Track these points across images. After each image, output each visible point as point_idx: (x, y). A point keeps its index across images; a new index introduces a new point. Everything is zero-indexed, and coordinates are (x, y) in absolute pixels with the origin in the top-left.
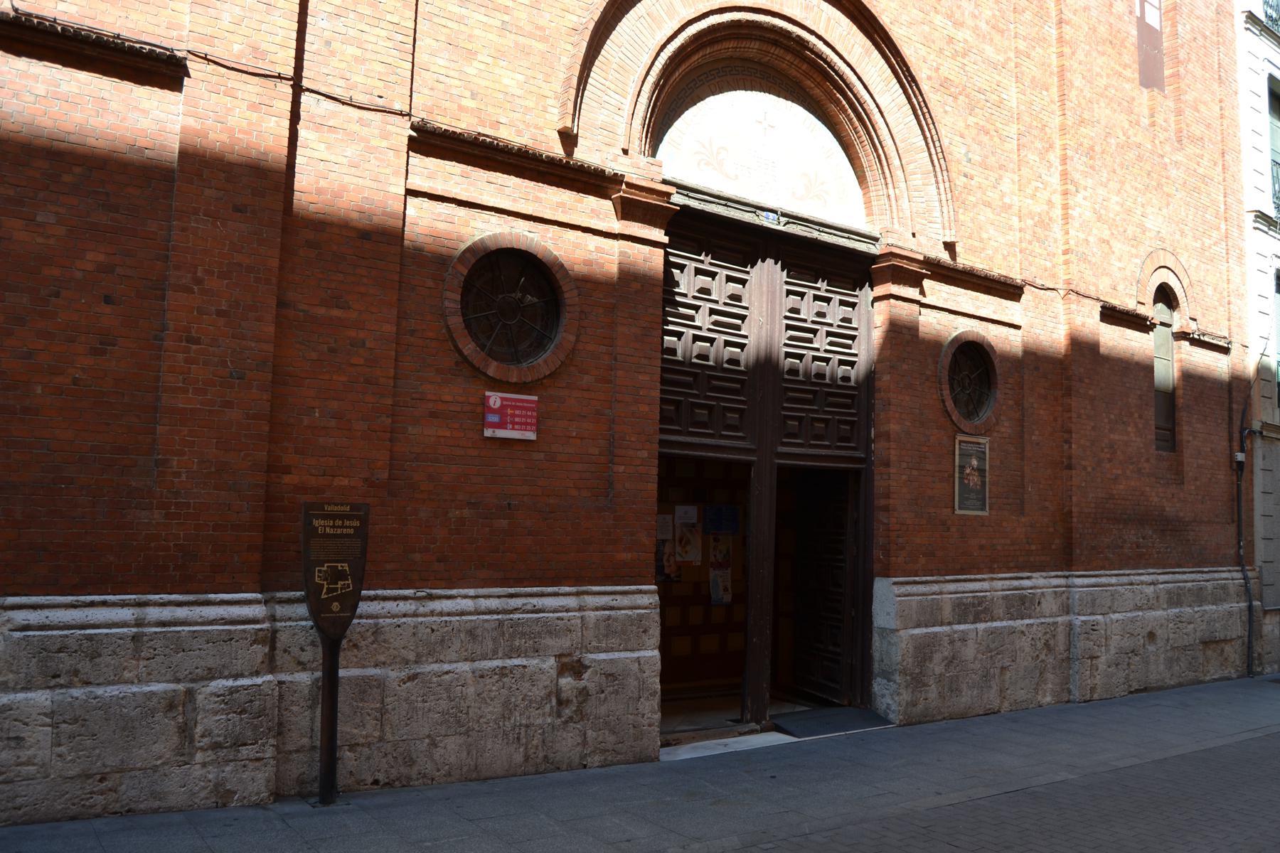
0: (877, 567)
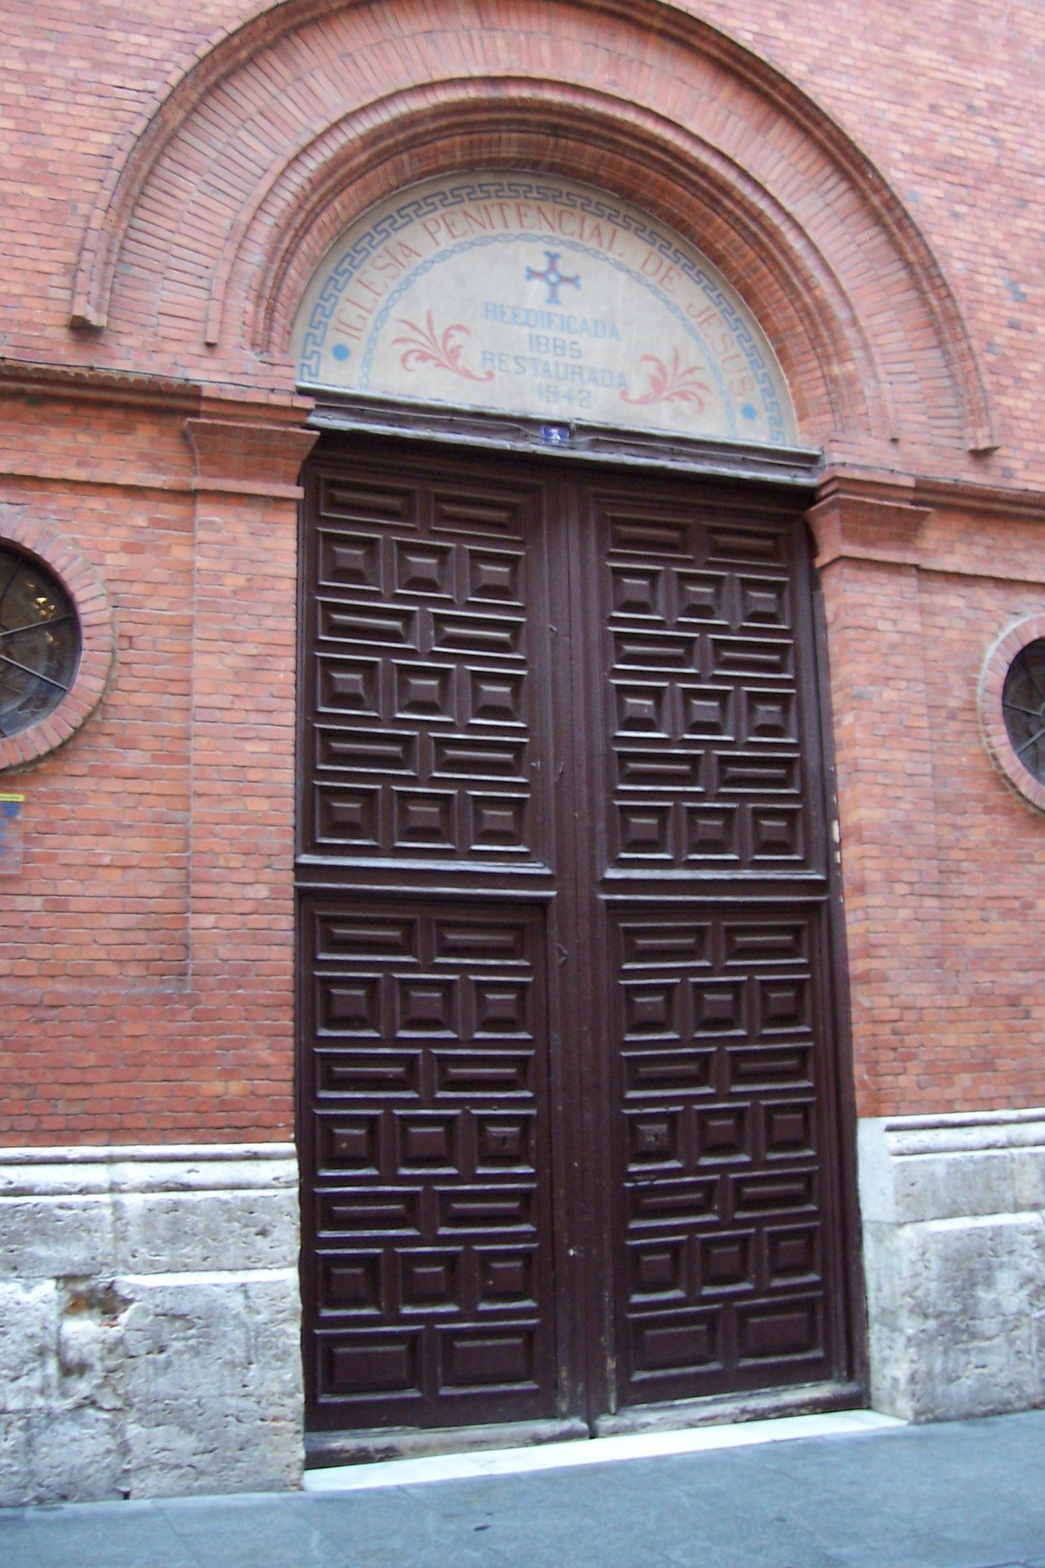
0: (860, 1098)
